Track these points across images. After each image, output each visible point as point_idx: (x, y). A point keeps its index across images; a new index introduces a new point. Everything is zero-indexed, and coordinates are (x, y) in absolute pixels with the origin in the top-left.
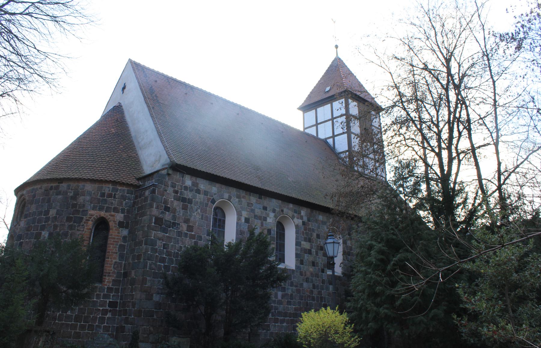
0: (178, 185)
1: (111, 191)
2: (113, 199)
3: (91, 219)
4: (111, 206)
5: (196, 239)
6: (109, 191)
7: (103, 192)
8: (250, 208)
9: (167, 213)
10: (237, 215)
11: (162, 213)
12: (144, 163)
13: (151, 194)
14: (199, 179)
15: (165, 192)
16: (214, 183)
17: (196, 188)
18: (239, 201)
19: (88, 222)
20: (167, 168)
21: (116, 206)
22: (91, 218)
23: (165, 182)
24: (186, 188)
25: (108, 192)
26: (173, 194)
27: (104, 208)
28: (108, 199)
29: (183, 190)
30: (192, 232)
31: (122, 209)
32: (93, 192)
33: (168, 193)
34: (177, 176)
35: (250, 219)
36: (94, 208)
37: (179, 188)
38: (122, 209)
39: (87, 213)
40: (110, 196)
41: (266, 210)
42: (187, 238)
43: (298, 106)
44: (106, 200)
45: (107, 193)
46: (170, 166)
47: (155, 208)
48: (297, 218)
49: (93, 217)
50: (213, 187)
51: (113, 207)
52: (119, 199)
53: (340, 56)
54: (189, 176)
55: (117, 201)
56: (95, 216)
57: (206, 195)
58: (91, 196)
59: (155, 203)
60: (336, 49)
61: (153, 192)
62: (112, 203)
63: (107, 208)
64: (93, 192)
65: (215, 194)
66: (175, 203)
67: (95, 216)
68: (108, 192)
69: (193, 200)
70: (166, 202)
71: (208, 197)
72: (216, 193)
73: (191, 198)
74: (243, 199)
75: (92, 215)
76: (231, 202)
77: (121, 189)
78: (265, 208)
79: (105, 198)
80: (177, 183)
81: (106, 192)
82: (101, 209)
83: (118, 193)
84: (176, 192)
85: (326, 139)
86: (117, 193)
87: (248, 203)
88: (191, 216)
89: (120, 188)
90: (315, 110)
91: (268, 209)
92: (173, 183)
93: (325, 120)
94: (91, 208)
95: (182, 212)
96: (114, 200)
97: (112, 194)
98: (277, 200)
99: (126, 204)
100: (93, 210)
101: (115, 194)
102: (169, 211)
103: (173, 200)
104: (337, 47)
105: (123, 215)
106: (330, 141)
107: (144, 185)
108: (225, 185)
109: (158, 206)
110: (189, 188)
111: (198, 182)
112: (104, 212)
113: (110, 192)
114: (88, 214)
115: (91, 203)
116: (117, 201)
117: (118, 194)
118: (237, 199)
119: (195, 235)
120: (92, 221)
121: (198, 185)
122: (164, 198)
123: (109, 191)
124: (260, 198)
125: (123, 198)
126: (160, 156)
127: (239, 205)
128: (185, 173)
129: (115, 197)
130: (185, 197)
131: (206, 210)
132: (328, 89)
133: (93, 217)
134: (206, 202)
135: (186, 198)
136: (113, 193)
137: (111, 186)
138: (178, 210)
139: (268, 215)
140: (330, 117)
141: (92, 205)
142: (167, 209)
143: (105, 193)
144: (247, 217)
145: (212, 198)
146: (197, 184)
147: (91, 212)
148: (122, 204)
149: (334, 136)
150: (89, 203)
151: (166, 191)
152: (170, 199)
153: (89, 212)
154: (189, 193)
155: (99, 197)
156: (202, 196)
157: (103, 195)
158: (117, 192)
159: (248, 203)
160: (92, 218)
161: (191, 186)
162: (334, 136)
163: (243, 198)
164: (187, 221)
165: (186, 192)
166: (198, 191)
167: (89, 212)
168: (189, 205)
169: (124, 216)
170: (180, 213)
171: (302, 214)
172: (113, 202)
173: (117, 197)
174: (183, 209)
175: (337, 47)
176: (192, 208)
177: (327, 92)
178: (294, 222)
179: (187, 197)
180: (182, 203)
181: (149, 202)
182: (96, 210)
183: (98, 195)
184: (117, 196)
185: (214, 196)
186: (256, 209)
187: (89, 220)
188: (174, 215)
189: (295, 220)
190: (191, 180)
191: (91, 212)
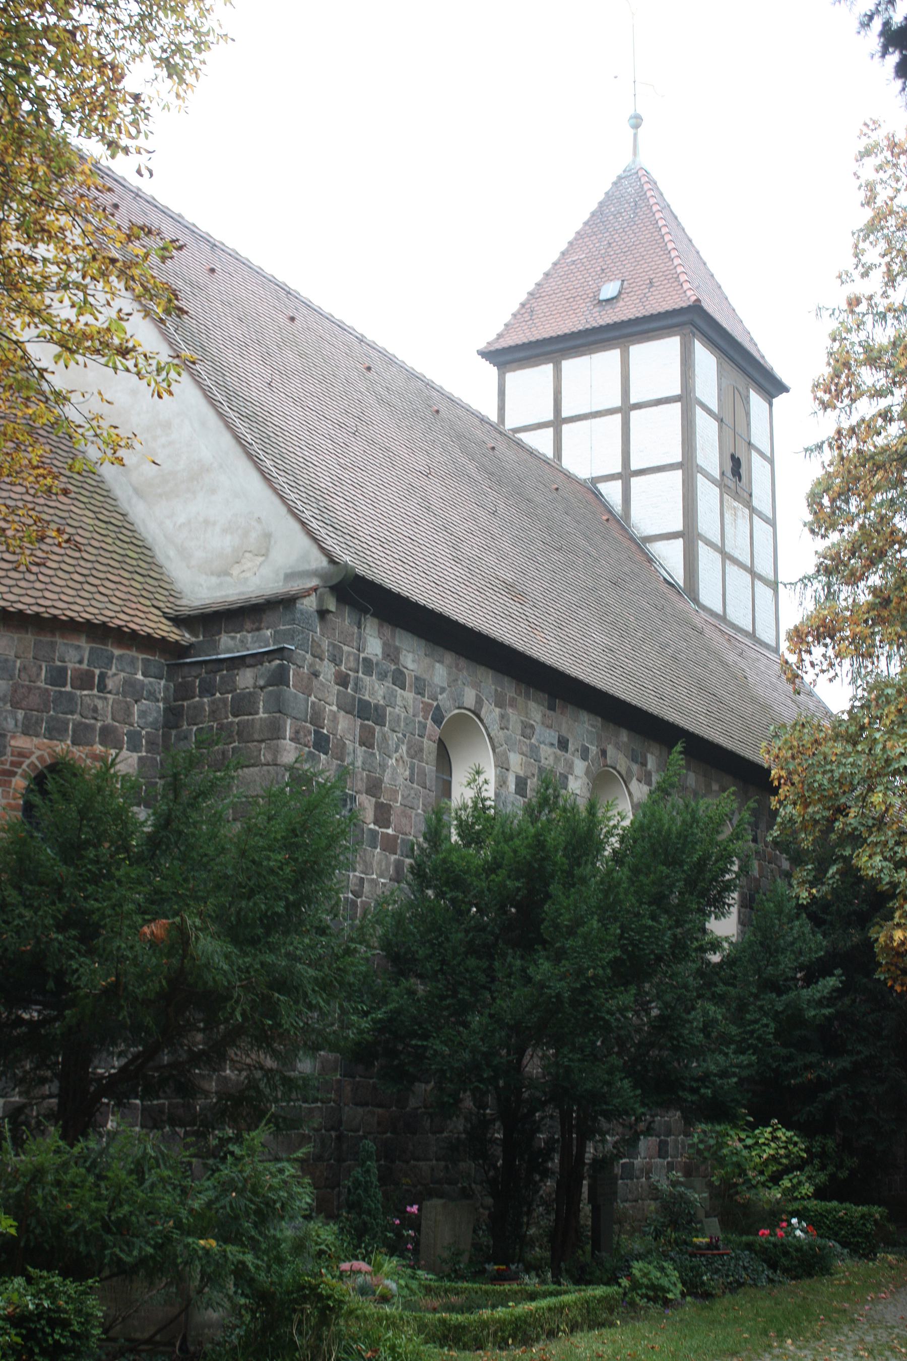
0: (349, 654)
1: (86, 661)
2: (95, 692)
3: (20, 771)
4: (93, 721)
5: (399, 852)
6: (81, 662)
7: (59, 664)
8: (528, 741)
9: (323, 756)
10: (496, 766)
11: (312, 757)
12: (172, 553)
13: (269, 684)
14: (402, 631)
15: (315, 682)
16: (441, 650)
17: (393, 667)
18: (502, 717)
19: (10, 782)
20: (315, 589)
21: (109, 721)
22: (19, 764)
23: (313, 640)
24: (368, 666)
25: (77, 666)
26: (337, 687)
27: (67, 730)
28: (78, 692)
29: (360, 675)
30: (388, 827)
31: (130, 734)
32: (18, 664)
33: (322, 684)
34: (344, 621)
35: (529, 781)
36: (28, 730)
37: (352, 664)
38: (130, 734)
39: (5, 747)
40: (84, 680)
41: (567, 751)
42: (376, 848)
43: (482, 345)
44: (71, 697)
45: (74, 670)
46: (334, 582)
47: (291, 740)
48: (639, 781)
49: (28, 762)
50: (437, 665)
51: (99, 724)
52: (117, 694)
53: (647, 161)
54: (376, 621)
55: (111, 702)
56: (33, 758)
57: (419, 693)
58: (12, 678)
59: (289, 721)
60: (632, 131)
61: (280, 678)
62: (95, 709)
63: (78, 726)
64: (18, 664)
65: (443, 690)
66: (341, 720)
67: (33, 758)
68: (77, 666)
69: (388, 709)
70: (316, 719)
71: (426, 700)
72: (445, 685)
73: (382, 702)
74: (510, 711)
75: (23, 754)
76: (481, 720)
77: (121, 656)
78: (563, 744)
79: (68, 688)
80: (345, 648)
81: (70, 665)
82: (55, 731)
83: (114, 670)
84: (342, 680)
85: (595, 480)
86: (110, 673)
87: (522, 722)
88: (383, 766)
89: (117, 652)
90: (551, 366)
91: (571, 747)
92: (334, 646)
93: (594, 409)
94: (16, 725)
95: (361, 750)
96: (100, 698)
97: (93, 672)
98: (592, 716)
99: (143, 714)
100: (26, 733)
101: (103, 676)
102: (326, 753)
103: (334, 708)
104: (636, 122)
105: (135, 756)
106: (612, 492)
107: (214, 647)
108: (457, 653)
109: (297, 732)
110: (377, 664)
111: (397, 644)
112: (69, 742)
113: (84, 666)
114: (9, 749)
115: (16, 705)
116: (111, 702)
117: (115, 675)
118: (497, 710)
119: (395, 838)
120: (25, 776)
121: (398, 653)
122: (313, 703)
123: (81, 662)
124: (552, 708)
125: (132, 690)
126: (268, 536)
127: (501, 732)
128: (365, 611)
129: (102, 688)
130: (367, 698)
131: (421, 750)
132: (609, 290)
133: (28, 762)
134: (421, 719)
135: (369, 703)
136: (97, 672)
137: (85, 645)
138: (350, 745)
139: (570, 766)
140: (617, 402)
141: (20, 714)
142: (322, 743)
143: (64, 670)
144: (522, 774)
145: (435, 704)
146: (398, 650)
147: (21, 742)
148: (129, 714)
149: (626, 475)
150: (8, 707)
151: (316, 675)
152: (328, 708)
153: (13, 743)
154: (377, 686)
155: (42, 685)
156: (409, 695)
157: (58, 677)
158: (109, 665)
159: (522, 722)
160: (24, 766)
161: (380, 656)
162: (626, 475)
163: (511, 706)
164: (374, 787)
165: (367, 679)
166: (399, 679)
167: (13, 743)
168: (377, 728)
169: (140, 758)
170: (357, 755)
171: (649, 766)
172: (100, 704)
173: (110, 687)
174: (362, 744)
175: (636, 122)
176: (385, 738)
177: (607, 301)
178: (630, 794)
179: (373, 701)
180: (359, 721)
181: (262, 715)
182: (37, 736)
183: (39, 675)
184: (110, 684)
185: (440, 697)
186: (542, 746)
187: (14, 774)
188: (339, 766)
189: (634, 785)
190: (381, 635)
191: (21, 742)
